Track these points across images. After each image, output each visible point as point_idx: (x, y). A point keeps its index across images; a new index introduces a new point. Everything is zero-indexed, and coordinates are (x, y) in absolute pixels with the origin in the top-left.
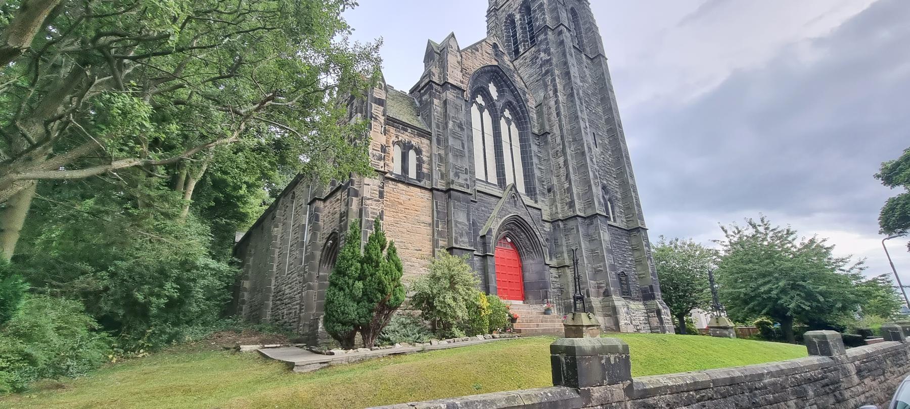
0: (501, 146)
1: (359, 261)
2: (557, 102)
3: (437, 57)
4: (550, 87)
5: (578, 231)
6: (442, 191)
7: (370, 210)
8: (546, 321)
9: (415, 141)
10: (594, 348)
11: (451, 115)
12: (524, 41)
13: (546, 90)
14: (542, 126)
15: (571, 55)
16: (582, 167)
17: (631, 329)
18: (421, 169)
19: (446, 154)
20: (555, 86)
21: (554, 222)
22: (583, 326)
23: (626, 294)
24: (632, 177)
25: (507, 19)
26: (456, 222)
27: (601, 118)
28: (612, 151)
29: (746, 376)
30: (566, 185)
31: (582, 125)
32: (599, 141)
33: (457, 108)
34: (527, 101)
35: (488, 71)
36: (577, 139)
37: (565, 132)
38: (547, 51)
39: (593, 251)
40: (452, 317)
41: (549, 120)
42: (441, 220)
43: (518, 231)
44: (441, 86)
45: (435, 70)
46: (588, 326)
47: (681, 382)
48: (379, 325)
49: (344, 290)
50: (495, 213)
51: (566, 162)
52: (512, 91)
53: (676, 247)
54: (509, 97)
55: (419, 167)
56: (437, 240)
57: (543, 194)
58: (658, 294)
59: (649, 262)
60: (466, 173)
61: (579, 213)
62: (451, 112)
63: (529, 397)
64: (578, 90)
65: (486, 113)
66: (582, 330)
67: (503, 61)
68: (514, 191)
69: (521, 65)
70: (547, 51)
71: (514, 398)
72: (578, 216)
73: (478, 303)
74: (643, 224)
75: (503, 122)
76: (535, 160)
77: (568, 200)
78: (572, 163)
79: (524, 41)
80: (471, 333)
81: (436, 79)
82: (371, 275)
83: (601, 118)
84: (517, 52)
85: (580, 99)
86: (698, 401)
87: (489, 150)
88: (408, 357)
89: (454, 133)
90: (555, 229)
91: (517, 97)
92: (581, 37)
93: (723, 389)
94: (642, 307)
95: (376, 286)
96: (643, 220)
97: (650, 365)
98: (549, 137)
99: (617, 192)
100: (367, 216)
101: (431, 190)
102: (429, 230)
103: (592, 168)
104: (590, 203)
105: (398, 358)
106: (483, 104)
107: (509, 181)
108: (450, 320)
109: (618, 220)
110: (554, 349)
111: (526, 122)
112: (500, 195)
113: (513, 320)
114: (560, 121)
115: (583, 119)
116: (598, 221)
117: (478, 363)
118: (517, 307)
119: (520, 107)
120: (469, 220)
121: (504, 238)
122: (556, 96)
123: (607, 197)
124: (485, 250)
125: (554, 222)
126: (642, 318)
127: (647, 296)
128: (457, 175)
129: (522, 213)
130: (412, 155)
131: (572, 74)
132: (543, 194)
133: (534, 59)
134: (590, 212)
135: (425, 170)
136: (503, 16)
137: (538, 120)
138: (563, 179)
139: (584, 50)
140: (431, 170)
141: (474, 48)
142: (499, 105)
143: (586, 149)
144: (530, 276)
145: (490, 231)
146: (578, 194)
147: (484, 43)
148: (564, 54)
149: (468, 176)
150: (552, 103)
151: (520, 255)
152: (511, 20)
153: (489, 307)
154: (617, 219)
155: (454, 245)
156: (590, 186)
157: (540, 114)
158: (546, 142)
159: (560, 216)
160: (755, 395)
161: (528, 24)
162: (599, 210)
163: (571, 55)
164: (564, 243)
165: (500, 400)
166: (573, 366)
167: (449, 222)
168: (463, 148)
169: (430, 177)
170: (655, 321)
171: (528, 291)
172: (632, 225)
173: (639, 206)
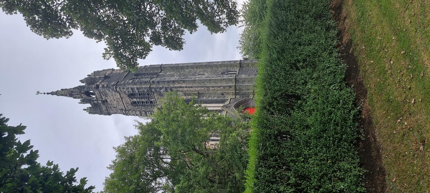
2: (186, 87)
4: (178, 89)
14: (195, 94)
16: (215, 81)
20: (178, 87)
21: (236, 94)
24: (218, 62)
25: (133, 105)
30: (222, 88)
36: (203, 81)
37: (199, 86)
38: (161, 89)
41: (193, 91)
51: (212, 87)
53: (243, 42)
61: (234, 85)
70: (161, 89)
74: (238, 61)
76: (210, 98)
78: (213, 85)
85: (186, 78)
92: (149, 73)
96: (236, 61)
98: (200, 92)
103: (215, 77)
104: (230, 80)
107: (220, 109)
109: (236, 70)
114: (194, 87)
122: (183, 87)
123: (226, 73)
125: (236, 94)
129: (233, 105)
134: (234, 81)
136: (130, 107)
138: (219, 89)
150: (186, 89)
156: (224, 79)
157: (189, 95)
158: (202, 93)
162: (233, 77)
163: (165, 79)
164: (245, 91)
172: (238, 65)
173: (230, 61)
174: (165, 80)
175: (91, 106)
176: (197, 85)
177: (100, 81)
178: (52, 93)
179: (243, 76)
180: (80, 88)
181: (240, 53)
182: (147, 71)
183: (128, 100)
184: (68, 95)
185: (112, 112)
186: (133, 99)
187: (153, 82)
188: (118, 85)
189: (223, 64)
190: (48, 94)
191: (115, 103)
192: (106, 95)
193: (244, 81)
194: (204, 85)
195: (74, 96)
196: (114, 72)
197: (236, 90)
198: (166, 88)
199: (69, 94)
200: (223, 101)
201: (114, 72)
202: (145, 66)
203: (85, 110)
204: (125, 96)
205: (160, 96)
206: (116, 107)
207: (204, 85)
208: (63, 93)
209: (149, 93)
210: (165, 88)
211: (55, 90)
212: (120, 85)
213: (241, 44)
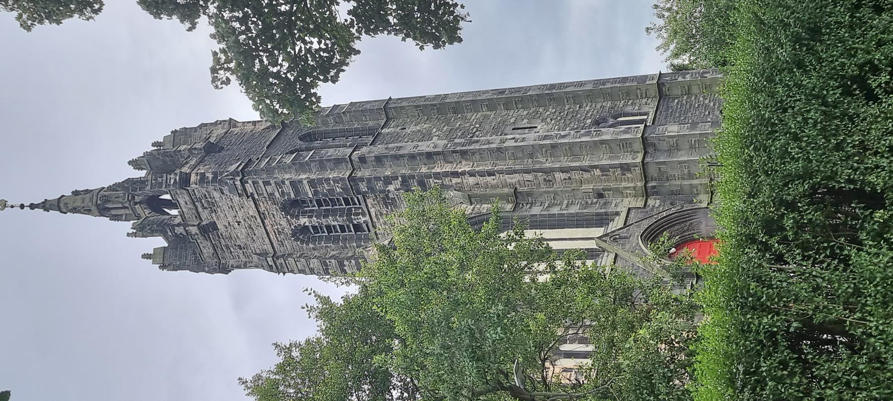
2: (472, 174)
4: (447, 181)
10: (170, 15)
14: (504, 198)
16: (572, 150)
20: (446, 174)
21: (647, 193)
25: (297, 240)
28: (539, 106)
30: (598, 172)
31: (512, 143)
32: (525, 123)
36: (532, 152)
37: (517, 167)
38: (388, 181)
51: (563, 170)
53: (669, 10)
57: (605, 204)
68: (607, 239)
70: (388, 181)
72: (643, 162)
74: (652, 77)
76: (555, 210)
77: (619, 171)
78: (565, 163)
83: (486, 117)
85: (471, 143)
90: (657, 193)
98: (520, 189)
103: (570, 137)
104: (625, 145)
107: (592, 245)
109: (645, 109)
112: (612, 256)
114: (501, 172)
116: (651, 136)
122: (463, 173)
123: (611, 121)
125: (647, 193)
129: (637, 232)
134: (638, 146)
136: (290, 245)
138: (586, 175)
146: (610, 158)
148: (397, 157)
150: (471, 180)
154: (643, 110)
156: (603, 142)
157: (484, 199)
158: (529, 194)
159: (640, 184)
162: (637, 132)
164: (678, 182)
172: (654, 91)
173: (624, 80)
174: (401, 152)
175: (166, 245)
176: (510, 164)
177: (192, 163)
179: (673, 129)
180: (130, 185)
181: (658, 48)
182: (342, 122)
183: (284, 222)
184: (93, 208)
185: (232, 262)
186: (297, 217)
187: (362, 159)
188: (249, 173)
189: (600, 91)
190: (32, 206)
191: (241, 233)
192: (212, 207)
193: (675, 146)
194: (534, 163)
195: (113, 212)
197: (646, 178)
198: (405, 181)
199: (97, 205)
200: (602, 220)
202: (335, 107)
203: (146, 256)
204: (274, 209)
206: (246, 247)
207: (534, 163)
208: (78, 204)
209: (350, 198)
211: (53, 196)
212: (256, 172)
213: (661, 16)
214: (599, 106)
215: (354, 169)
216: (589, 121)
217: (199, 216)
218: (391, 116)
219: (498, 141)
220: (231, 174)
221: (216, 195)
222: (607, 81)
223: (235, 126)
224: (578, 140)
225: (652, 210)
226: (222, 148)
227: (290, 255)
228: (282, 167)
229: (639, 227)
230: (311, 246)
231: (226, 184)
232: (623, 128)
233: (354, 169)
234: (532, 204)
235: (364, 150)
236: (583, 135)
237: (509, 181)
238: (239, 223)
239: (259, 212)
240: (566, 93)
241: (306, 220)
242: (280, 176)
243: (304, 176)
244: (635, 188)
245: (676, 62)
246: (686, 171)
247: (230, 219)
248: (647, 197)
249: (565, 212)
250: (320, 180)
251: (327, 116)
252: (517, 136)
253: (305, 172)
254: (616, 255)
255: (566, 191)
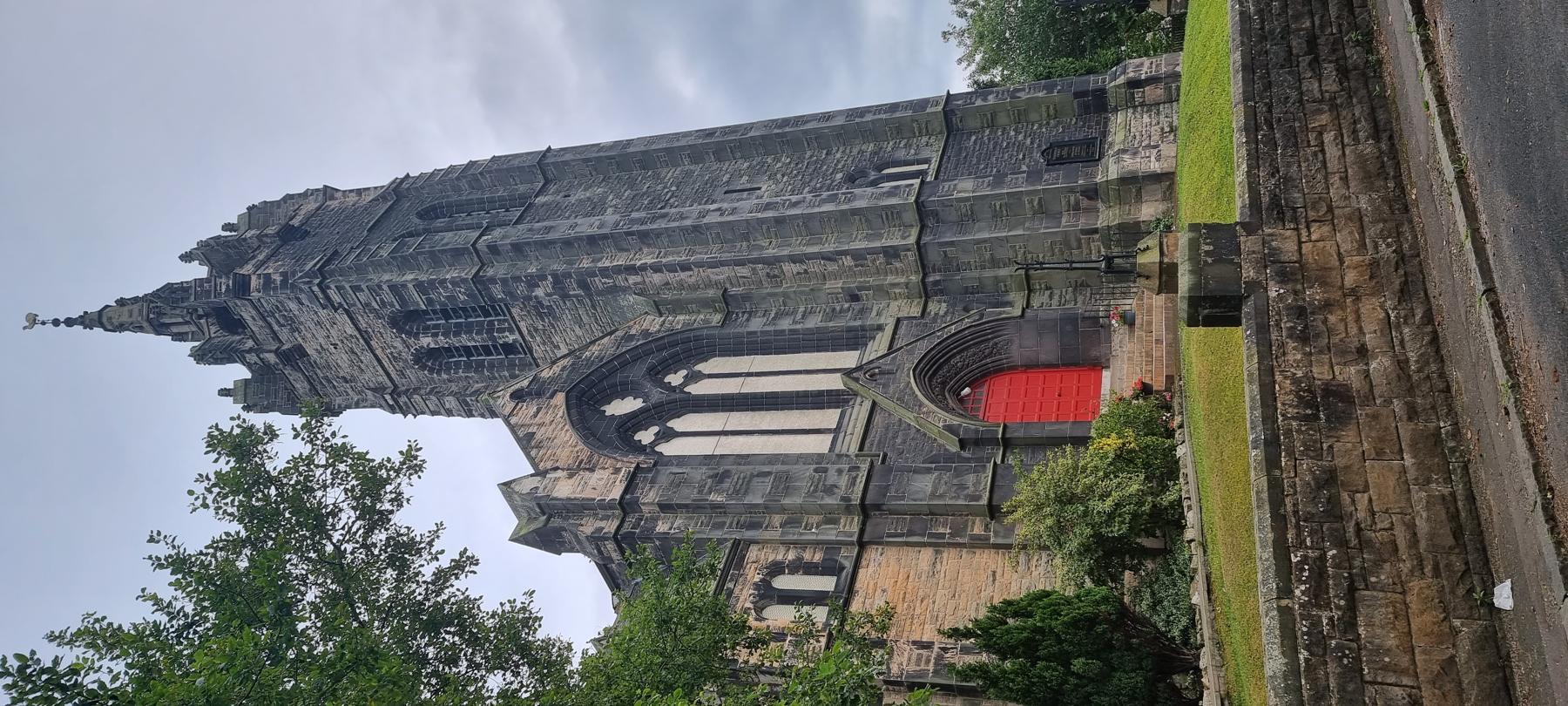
0: (746, 396)
1: (1033, 665)
2: (657, 269)
3: (556, 522)
4: (620, 280)
5: (952, 243)
6: (864, 524)
7: (912, 668)
8: (1150, 323)
9: (753, 575)
11: (695, 495)
12: (490, 331)
13: (625, 290)
14: (706, 304)
15: (549, 229)
16: (810, 226)
17: (1168, 149)
18: (816, 566)
19: (783, 510)
20: (618, 270)
21: (926, 293)
22: (1161, 262)
23: (1091, 151)
24: (828, 116)
25: (423, 367)
26: (933, 495)
27: (689, 174)
28: (767, 154)
29: (1242, 43)
30: (848, 261)
33: (679, 483)
34: (646, 333)
35: (581, 414)
36: (746, 231)
37: (726, 256)
38: (532, 282)
39: (996, 215)
40: (1141, 504)
41: (695, 287)
42: (929, 528)
43: (950, 371)
44: (625, 514)
45: (588, 527)
46: (1162, 253)
47: (1244, 151)
48: (1156, 638)
49: (1091, 694)
50: (909, 418)
51: (794, 259)
52: (624, 364)
54: (638, 372)
55: (810, 569)
56: (973, 537)
58: (1093, 81)
59: (1023, 95)
60: (825, 470)
61: (912, 240)
62: (688, 495)
63: (1250, 357)
64: (633, 222)
65: (677, 424)
66: (1169, 265)
67: (553, 380)
69: (548, 340)
71: (1250, 375)
72: (918, 242)
73: (1111, 455)
74: (936, 101)
75: (696, 389)
76: (785, 324)
77: (881, 259)
78: (799, 247)
79: (490, 331)
80: (1171, 470)
81: (610, 527)
82: (1060, 641)
83: (689, 174)
84: (509, 349)
85: (654, 219)
86: (1271, 127)
87: (764, 419)
88: (1214, 569)
89: (737, 492)
90: (942, 292)
91: (637, 355)
92: (491, 200)
93: (1258, 86)
94: (1120, 117)
95: (1082, 633)
97: (1221, 191)
98: (733, 290)
99: (861, 152)
100: (924, 673)
101: (862, 545)
102: (949, 556)
103: (809, 204)
104: (891, 216)
105: (1215, 587)
106: (655, 429)
107: (835, 383)
108: (1146, 508)
109: (925, 154)
110: (1192, 322)
111: (697, 338)
112: (867, 405)
113: (1145, 390)
114: (700, 265)
115: (703, 215)
117: (1221, 441)
118: (1117, 381)
119: (660, 349)
120: (929, 471)
121: (961, 400)
122: (643, 268)
123: (873, 175)
124: (993, 441)
125: (926, 293)
126: (1146, 119)
127: (1097, 105)
128: (830, 490)
129: (908, 362)
130: (783, 582)
131: (594, 231)
132: (862, 311)
133: (540, 310)
134: (911, 216)
135: (818, 557)
136: (414, 375)
137: (690, 313)
138: (832, 267)
139: (523, 197)
140: (816, 544)
141: (527, 442)
142: (657, 395)
143: (770, 214)
144: (1048, 350)
145: (950, 429)
146: (868, 238)
147: (513, 420)
149: (832, 469)
150: (657, 278)
151: (999, 371)
152: (426, 358)
153: (1120, 435)
155: (984, 501)
156: (855, 212)
157: (678, 307)
158: (746, 297)
159: (915, 279)
160: (1272, 32)
161: (447, 316)
163: (549, 229)
164: (975, 274)
165: (1251, 391)
166: (1214, 300)
167: (933, 512)
168: (769, 473)
169: (831, 547)
170: (1153, 93)
171: (1082, 351)
172: (938, 124)
173: (894, 107)
174: (550, 236)
175: (248, 375)
176: (714, 252)
177: (261, 257)
178: (87, 321)
179: (965, 187)
180: (172, 294)
181: (960, 61)
182: (481, 188)
183: (398, 344)
184: (145, 324)
185: (339, 400)
186: (416, 336)
187: (493, 249)
188: (332, 273)
189: (859, 127)
190: (70, 322)
191: (342, 359)
192: (293, 324)
193: (969, 213)
194: (750, 248)
195: (175, 330)
196: (333, 204)
197: (924, 267)
198: (558, 280)
199: (149, 320)
200: (855, 339)
201: (333, 204)
202: (472, 164)
203: (224, 392)
204: (379, 325)
205: (541, 316)
206: (353, 379)
207: (750, 248)
208: (125, 318)
209: (485, 306)
210: (555, 276)
211: (94, 308)
212: (342, 273)
213: (962, 15)
214: (855, 151)
215: (483, 265)
216: (839, 176)
217: (276, 337)
218: (550, 176)
219: (695, 215)
220: (307, 275)
221: (293, 306)
222: (867, 110)
223: (332, 198)
224: (817, 210)
225: (934, 320)
226: (307, 233)
227: (416, 390)
228: (380, 266)
229: (911, 352)
230: (445, 376)
231: (301, 290)
232: (888, 185)
233: (483, 265)
234: (750, 313)
235: (498, 232)
236: (824, 201)
237: (714, 278)
238: (335, 346)
239: (358, 329)
240: (805, 132)
241: (429, 340)
242: (374, 278)
243: (410, 277)
244: (907, 285)
245: (985, 78)
246: (987, 256)
247: (321, 340)
248: (927, 297)
249: (798, 326)
250: (431, 282)
251: (458, 179)
252: (725, 205)
253: (412, 269)
254: (874, 404)
255: (802, 292)
